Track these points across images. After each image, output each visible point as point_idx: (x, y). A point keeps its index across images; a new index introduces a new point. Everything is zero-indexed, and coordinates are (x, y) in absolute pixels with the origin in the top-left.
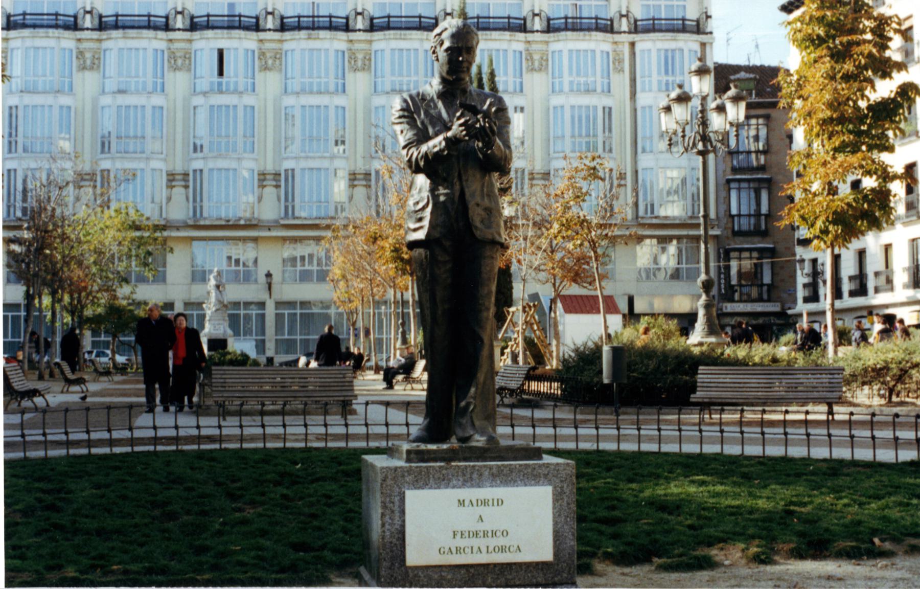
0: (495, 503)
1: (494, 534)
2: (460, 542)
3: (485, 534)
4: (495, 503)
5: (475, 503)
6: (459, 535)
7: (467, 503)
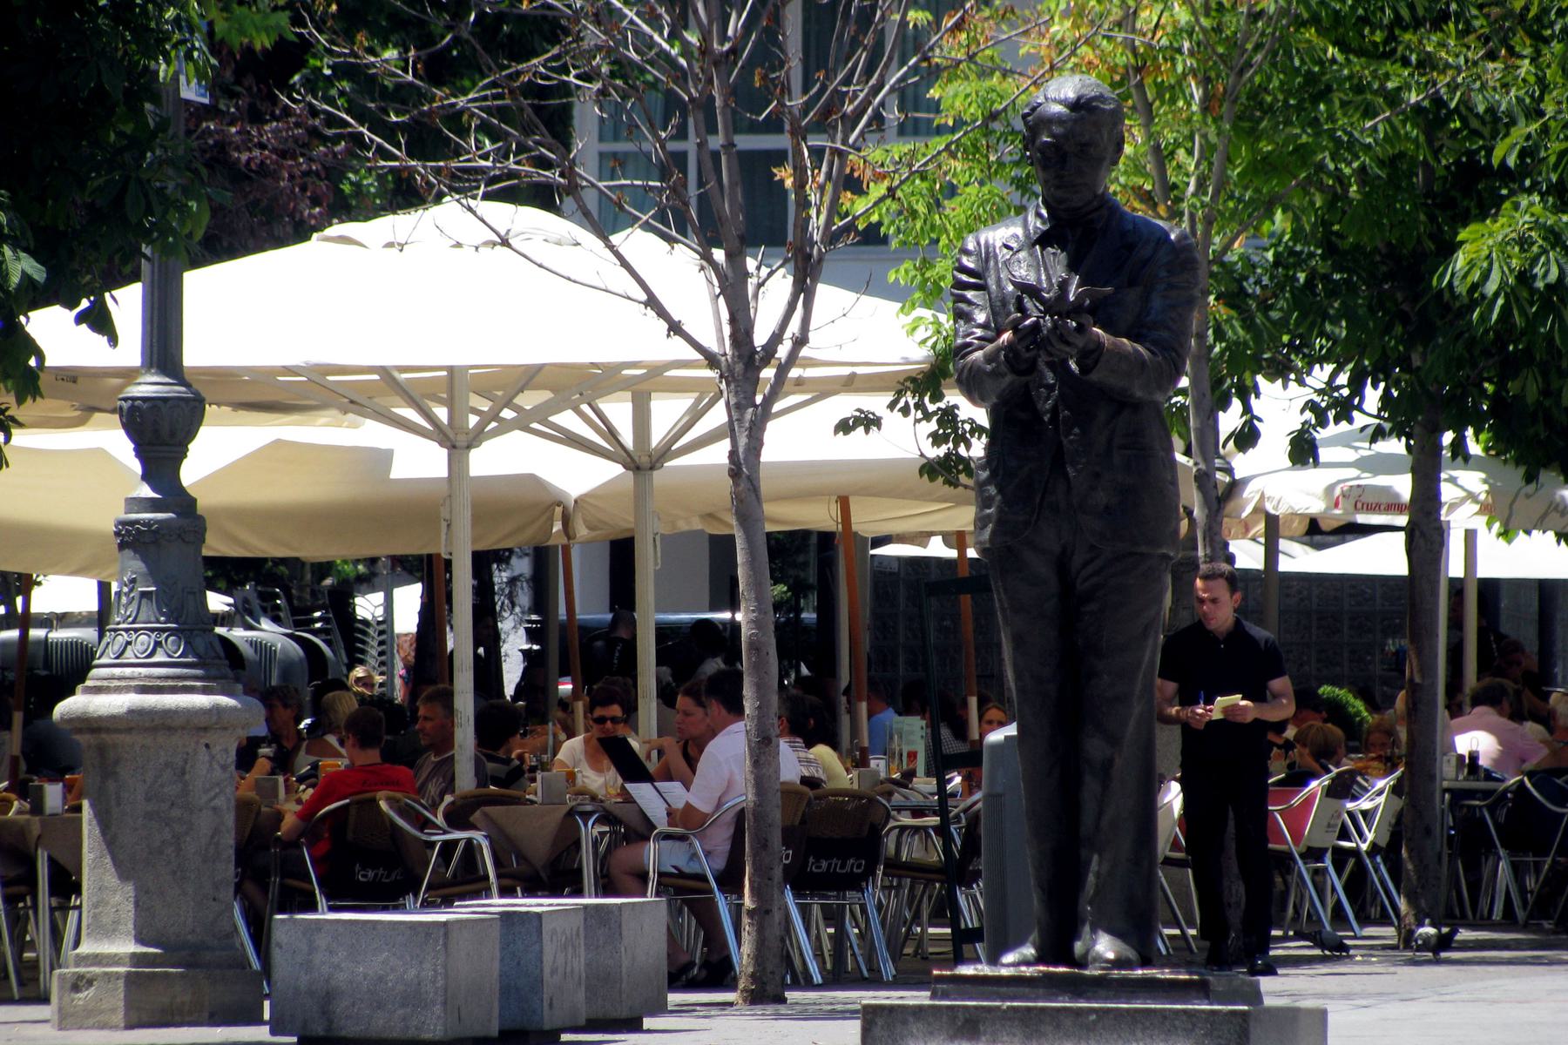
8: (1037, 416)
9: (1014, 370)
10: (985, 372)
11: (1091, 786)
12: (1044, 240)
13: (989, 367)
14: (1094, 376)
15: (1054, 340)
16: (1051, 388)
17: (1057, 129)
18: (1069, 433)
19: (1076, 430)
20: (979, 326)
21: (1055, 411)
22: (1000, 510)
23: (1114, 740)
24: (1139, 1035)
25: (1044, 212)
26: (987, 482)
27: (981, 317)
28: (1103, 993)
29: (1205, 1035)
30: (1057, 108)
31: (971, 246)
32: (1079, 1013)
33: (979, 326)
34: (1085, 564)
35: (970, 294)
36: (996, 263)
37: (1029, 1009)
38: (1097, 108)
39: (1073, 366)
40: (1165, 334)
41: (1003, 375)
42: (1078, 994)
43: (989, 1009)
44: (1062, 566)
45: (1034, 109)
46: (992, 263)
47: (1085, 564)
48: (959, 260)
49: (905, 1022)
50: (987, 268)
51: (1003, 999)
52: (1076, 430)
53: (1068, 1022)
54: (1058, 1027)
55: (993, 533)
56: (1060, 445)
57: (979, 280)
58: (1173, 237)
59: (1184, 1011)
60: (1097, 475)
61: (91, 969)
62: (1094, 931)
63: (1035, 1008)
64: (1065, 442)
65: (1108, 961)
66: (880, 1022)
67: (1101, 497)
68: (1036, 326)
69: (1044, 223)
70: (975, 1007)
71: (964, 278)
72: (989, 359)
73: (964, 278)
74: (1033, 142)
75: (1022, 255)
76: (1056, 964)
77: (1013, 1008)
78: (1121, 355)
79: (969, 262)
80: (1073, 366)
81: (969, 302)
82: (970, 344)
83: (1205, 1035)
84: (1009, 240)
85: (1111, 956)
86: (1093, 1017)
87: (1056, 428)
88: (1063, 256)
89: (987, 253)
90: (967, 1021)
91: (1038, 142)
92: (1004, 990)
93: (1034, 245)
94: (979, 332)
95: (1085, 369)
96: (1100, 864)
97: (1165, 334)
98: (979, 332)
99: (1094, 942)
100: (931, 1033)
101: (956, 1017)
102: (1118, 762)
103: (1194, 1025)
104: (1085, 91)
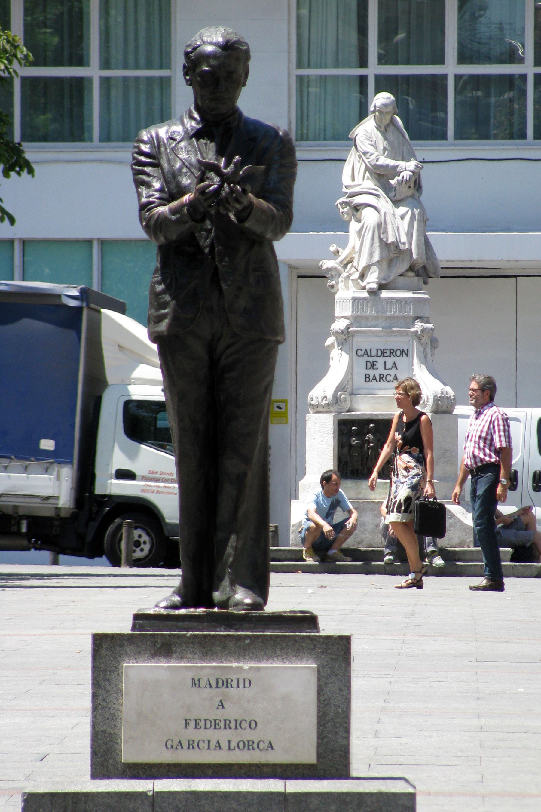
0: (241, 685)
1: (239, 724)
2: (192, 733)
3: (227, 724)
4: (241, 685)
5: (214, 683)
6: (192, 724)
7: (203, 682)
8: (200, 250)
9: (193, 220)
10: (170, 220)
11: (227, 492)
12: (198, 135)
13: (173, 218)
14: (247, 224)
15: (230, 200)
16: (209, 231)
17: (213, 62)
18: (221, 261)
19: (227, 259)
20: (157, 190)
21: (212, 247)
22: (175, 311)
23: (247, 460)
24: (278, 652)
25: (196, 115)
26: (163, 292)
27: (157, 185)
28: (246, 625)
29: (323, 652)
30: (210, 48)
31: (145, 138)
32: (239, 638)
33: (157, 190)
34: (228, 347)
35: (148, 169)
36: (166, 149)
37: (205, 636)
38: (237, 48)
39: (232, 217)
40: (281, 197)
41: (185, 223)
42: (229, 627)
43: (178, 636)
44: (211, 349)
45: (195, 49)
46: (163, 149)
47: (228, 347)
48: (138, 147)
49: (122, 646)
50: (160, 153)
51: (187, 630)
52: (227, 259)
53: (231, 645)
54: (224, 647)
55: (170, 326)
56: (216, 268)
57: (154, 159)
58: (281, 133)
59: (309, 637)
60: (240, 288)
61: (290, 634)
62: (233, 584)
63: (209, 635)
64: (220, 267)
65: (248, 605)
66: (105, 646)
67: (242, 303)
68: (217, 191)
69: (198, 123)
70: (169, 635)
71: (143, 159)
72: (173, 212)
73: (143, 159)
74: (194, 70)
75: (182, 144)
76: (196, 606)
77: (194, 635)
78: (262, 211)
79: (145, 148)
80: (232, 217)
81: (148, 175)
82: (153, 202)
83: (323, 652)
84: (176, 131)
85: (248, 601)
86: (248, 641)
87: (213, 258)
88: (212, 146)
89: (159, 143)
90: (163, 644)
91: (198, 70)
92: (180, 624)
93: (191, 138)
94: (157, 195)
95: (241, 219)
96: (237, 541)
97: (281, 197)
98: (157, 195)
99: (235, 593)
100: (139, 653)
101: (156, 642)
102: (250, 475)
103: (315, 646)
104: (230, 37)
